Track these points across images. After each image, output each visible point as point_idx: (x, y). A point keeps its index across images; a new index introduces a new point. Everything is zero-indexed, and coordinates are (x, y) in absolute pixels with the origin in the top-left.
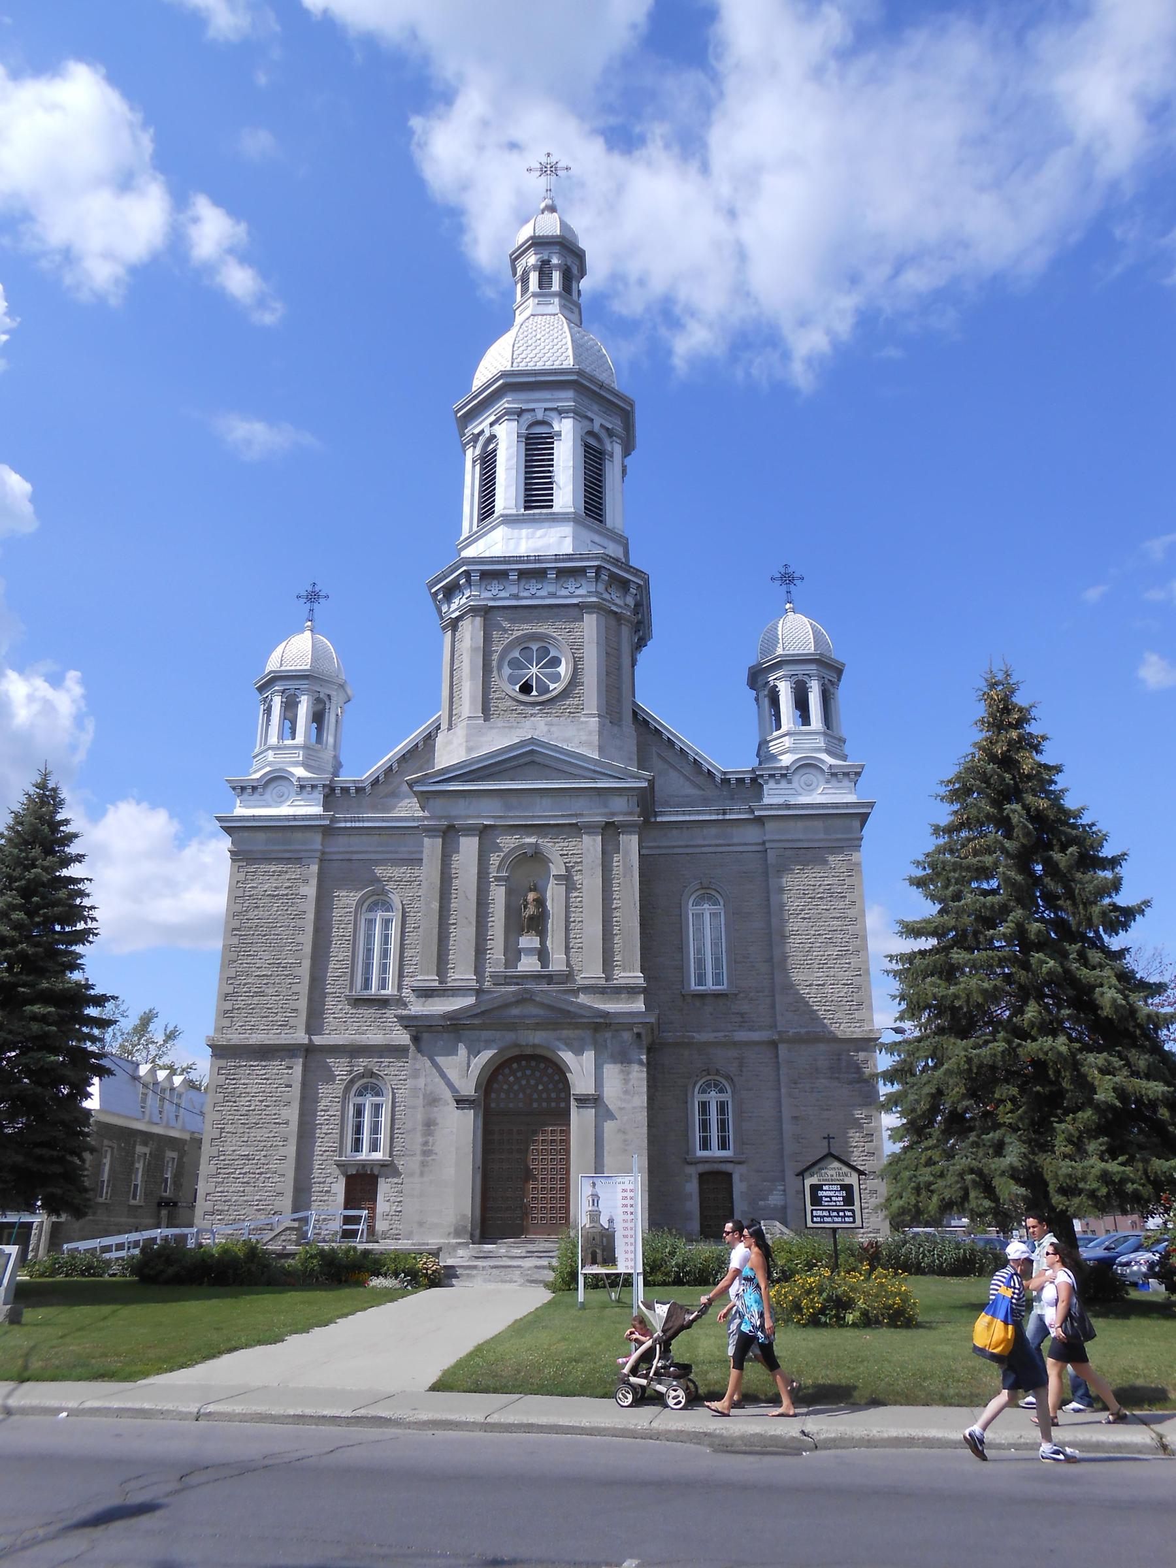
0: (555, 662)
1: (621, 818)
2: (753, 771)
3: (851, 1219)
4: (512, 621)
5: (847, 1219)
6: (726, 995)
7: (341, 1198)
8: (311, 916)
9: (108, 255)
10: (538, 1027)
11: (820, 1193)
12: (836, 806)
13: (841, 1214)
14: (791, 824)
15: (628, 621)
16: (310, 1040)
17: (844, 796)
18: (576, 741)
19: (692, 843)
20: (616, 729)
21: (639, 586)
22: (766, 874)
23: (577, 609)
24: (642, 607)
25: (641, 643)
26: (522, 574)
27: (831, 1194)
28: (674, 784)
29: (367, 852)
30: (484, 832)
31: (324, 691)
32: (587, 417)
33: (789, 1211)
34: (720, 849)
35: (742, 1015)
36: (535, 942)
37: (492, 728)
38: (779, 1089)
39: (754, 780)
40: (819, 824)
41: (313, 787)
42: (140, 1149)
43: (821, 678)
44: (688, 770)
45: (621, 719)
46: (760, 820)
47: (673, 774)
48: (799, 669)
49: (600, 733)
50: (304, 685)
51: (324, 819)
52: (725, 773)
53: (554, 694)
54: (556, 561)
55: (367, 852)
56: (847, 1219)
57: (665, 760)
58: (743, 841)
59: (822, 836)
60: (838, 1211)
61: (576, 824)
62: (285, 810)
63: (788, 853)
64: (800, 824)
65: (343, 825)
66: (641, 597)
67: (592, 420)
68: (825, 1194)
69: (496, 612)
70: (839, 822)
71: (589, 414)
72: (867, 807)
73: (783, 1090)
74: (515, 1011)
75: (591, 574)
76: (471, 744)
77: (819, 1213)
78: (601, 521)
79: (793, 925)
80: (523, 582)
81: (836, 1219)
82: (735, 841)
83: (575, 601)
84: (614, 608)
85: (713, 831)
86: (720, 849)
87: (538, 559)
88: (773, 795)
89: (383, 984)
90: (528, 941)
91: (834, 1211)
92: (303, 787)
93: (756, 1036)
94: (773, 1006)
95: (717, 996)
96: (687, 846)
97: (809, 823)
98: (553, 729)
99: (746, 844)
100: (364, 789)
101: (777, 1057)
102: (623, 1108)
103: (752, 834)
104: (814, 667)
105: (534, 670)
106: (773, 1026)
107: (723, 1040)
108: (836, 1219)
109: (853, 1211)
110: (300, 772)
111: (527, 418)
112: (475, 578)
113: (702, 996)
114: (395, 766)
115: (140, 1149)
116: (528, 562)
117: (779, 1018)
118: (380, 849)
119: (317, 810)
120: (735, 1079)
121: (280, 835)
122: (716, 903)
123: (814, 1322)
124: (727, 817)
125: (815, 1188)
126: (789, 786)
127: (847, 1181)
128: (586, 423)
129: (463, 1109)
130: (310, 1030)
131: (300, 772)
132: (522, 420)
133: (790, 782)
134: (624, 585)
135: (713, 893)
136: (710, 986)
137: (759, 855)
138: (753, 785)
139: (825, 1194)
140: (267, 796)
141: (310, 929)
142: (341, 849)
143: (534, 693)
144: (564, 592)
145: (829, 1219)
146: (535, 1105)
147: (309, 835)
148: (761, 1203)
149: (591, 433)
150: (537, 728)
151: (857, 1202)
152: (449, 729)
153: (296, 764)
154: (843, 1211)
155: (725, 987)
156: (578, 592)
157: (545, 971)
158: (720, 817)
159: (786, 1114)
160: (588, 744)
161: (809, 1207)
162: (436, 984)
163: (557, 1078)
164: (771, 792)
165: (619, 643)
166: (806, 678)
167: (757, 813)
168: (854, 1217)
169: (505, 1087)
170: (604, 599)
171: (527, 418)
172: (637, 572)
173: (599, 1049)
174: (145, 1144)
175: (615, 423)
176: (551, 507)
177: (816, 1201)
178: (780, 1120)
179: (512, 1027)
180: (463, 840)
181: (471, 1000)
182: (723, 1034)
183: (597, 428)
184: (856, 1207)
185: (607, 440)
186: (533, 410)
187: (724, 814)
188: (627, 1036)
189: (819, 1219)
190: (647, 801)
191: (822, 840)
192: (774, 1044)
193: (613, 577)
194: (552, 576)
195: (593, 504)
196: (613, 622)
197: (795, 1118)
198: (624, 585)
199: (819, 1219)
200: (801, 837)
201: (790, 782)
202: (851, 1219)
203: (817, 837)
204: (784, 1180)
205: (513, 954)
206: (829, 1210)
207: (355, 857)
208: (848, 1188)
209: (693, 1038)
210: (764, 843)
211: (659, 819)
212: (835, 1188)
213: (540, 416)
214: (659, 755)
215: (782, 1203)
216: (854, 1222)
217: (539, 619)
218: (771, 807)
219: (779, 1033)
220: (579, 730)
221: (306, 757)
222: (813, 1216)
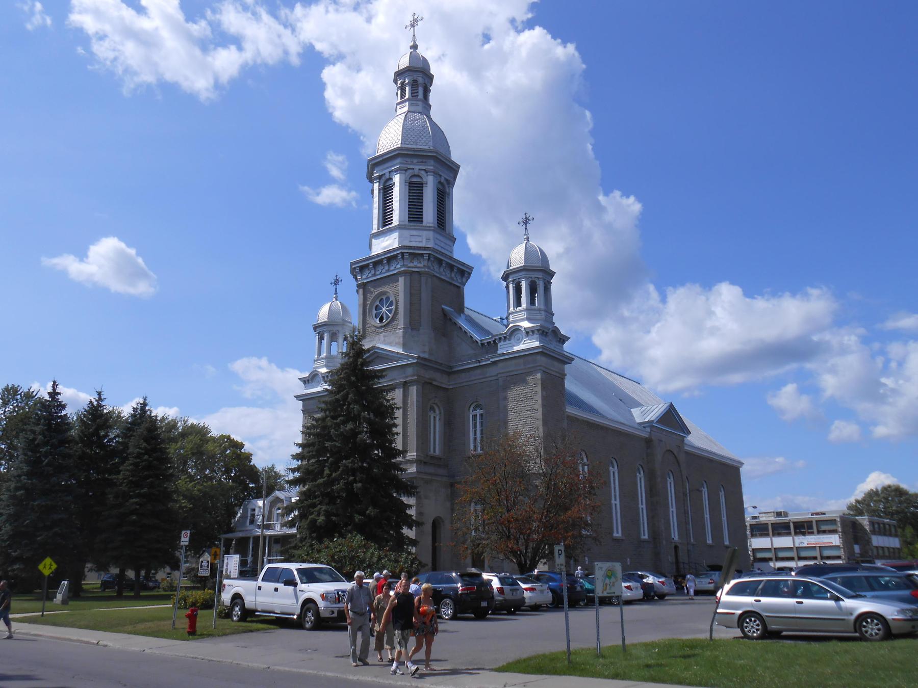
4: (374, 287)
9: (526, 13)
12: (530, 349)
31: (335, 329)
41: (533, 332)
43: (526, 278)
48: (533, 275)
49: (404, 337)
50: (325, 328)
62: (522, 347)
64: (514, 362)
79: (511, 416)
82: (488, 375)
89: (476, 450)
92: (529, 332)
104: (523, 273)
110: (526, 324)
111: (410, 172)
112: (406, 256)
119: (537, 344)
123: (223, 618)
131: (526, 324)
140: (512, 341)
153: (523, 320)
160: (397, 344)
171: (410, 172)
217: (384, 284)
218: (503, 354)
221: (327, 362)
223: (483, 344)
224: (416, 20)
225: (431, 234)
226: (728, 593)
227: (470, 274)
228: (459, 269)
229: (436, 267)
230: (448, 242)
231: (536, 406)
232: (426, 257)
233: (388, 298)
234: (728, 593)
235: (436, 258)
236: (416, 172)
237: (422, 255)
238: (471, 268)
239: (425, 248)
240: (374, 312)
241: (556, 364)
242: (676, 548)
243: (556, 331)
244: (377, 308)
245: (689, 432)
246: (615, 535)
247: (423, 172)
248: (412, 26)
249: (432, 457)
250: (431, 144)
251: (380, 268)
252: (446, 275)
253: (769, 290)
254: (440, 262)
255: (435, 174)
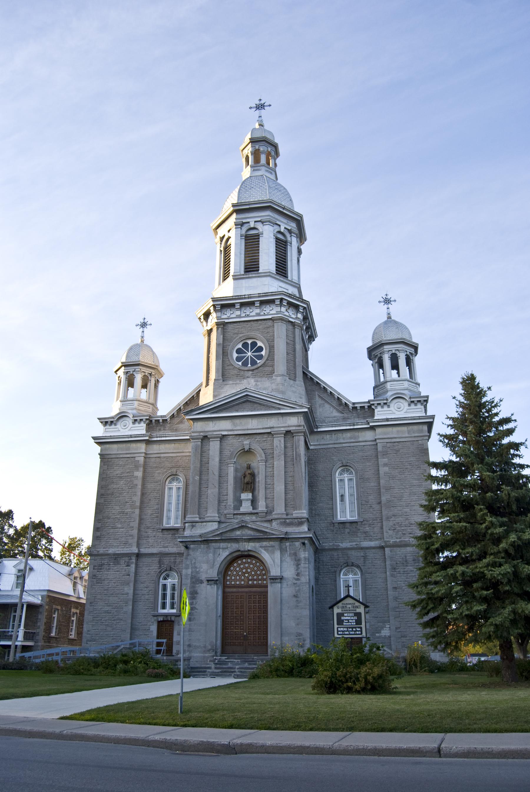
0: (260, 349)
1: (294, 428)
2: (369, 402)
3: (360, 633)
5: (357, 633)
6: (356, 522)
7: (155, 633)
8: (140, 487)
10: (250, 540)
11: (343, 618)
13: (354, 629)
14: (390, 429)
15: (298, 326)
16: (139, 551)
17: (417, 412)
18: (270, 389)
19: (337, 442)
20: (292, 382)
21: (304, 308)
22: (377, 457)
23: (271, 321)
24: (308, 317)
25: (312, 338)
26: (242, 305)
27: (349, 618)
28: (325, 411)
29: (168, 453)
30: (223, 437)
32: (277, 224)
33: (392, 639)
34: (352, 444)
35: (365, 533)
36: (250, 496)
37: (226, 384)
38: (386, 573)
39: (369, 407)
40: (405, 428)
42: (73, 610)
44: (335, 403)
45: (295, 377)
46: (373, 428)
47: (327, 406)
51: (146, 436)
52: (354, 404)
53: (259, 365)
54: (259, 297)
55: (168, 453)
56: (357, 633)
57: (322, 399)
58: (364, 439)
59: (407, 435)
60: (352, 628)
61: (270, 433)
63: (388, 445)
64: (395, 429)
65: (156, 439)
66: (307, 313)
67: (280, 226)
68: (345, 618)
69: (229, 325)
70: (415, 427)
71: (278, 223)
72: (430, 418)
73: (388, 573)
74: (238, 533)
75: (278, 302)
76: (216, 393)
77: (342, 629)
78: (285, 277)
80: (243, 309)
81: (351, 633)
82: (360, 439)
83: (270, 317)
84: (291, 320)
85: (348, 435)
86: (352, 444)
87: (250, 296)
88: (380, 414)
90: (246, 496)
91: (350, 628)
93: (373, 544)
94: (382, 528)
95: (352, 523)
96: (335, 444)
97: (411, 427)
98: (259, 383)
99: (366, 441)
100: (166, 420)
101: (385, 555)
102: (296, 583)
103: (369, 435)
105: (249, 354)
106: (382, 538)
107: (355, 546)
108: (351, 633)
109: (361, 628)
112: (285, 303)
113: (343, 523)
114: (182, 408)
115: (73, 610)
116: (245, 298)
117: (385, 534)
118: (175, 451)
120: (362, 567)
121: (173, 445)
122: (351, 473)
124: (356, 427)
125: (339, 615)
126: (389, 409)
127: (358, 610)
128: (276, 227)
129: (211, 585)
130: (138, 546)
132: (243, 228)
133: (389, 406)
134: (296, 307)
135: (350, 468)
136: (348, 517)
137: (373, 447)
138: (367, 410)
139: (345, 618)
140: (118, 426)
141: (139, 494)
142: (155, 452)
143: (249, 365)
144: (225, 317)
145: (347, 633)
146: (250, 582)
147: (139, 445)
148: (377, 635)
149: (279, 232)
150: (250, 384)
151: (363, 623)
152: (206, 387)
154: (355, 628)
155: (356, 518)
156: (271, 312)
157: (255, 511)
158: (352, 427)
159: (390, 586)
161: (336, 626)
162: (198, 519)
163: (261, 568)
164: (379, 413)
165: (294, 337)
166: (397, 352)
167: (371, 424)
168: (361, 631)
169: (235, 573)
170: (285, 315)
172: (304, 301)
173: (283, 551)
174: (77, 608)
175: (293, 226)
176: (259, 270)
177: (340, 622)
178: (387, 589)
179: (236, 540)
180: (211, 443)
181: (215, 526)
182: (355, 543)
183: (282, 230)
184: (363, 626)
185: (288, 235)
186: (249, 222)
187: (354, 425)
188: (298, 544)
189: (341, 633)
190: (309, 418)
191: (407, 437)
192: (382, 548)
193: (290, 304)
194: (257, 304)
195: (282, 269)
196: (291, 327)
197: (395, 588)
198: (296, 307)
199: (341, 633)
200: (395, 436)
201: (389, 406)
202: (360, 633)
203: (404, 436)
204: (389, 622)
205: (239, 502)
206: (347, 628)
207: (162, 455)
208: (359, 615)
209: (339, 545)
210: (375, 440)
211: (319, 430)
212: (351, 615)
213: (252, 225)
214: (319, 396)
215: (389, 634)
216: (361, 634)
218: (378, 420)
219: (385, 542)
220: (272, 383)
222: (338, 631)
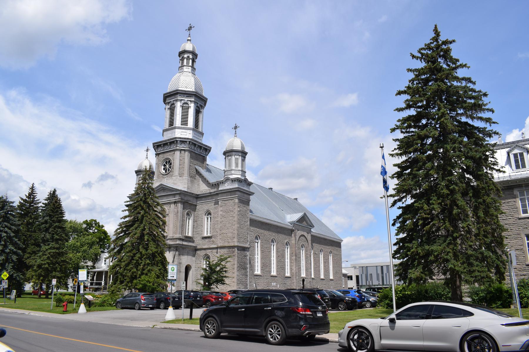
89: (207, 234)
112: (178, 142)
218: (221, 190)
223: (213, 185)
224: (191, 27)
225: (191, 132)
226: (396, 310)
227: (210, 151)
228: (204, 148)
229: (193, 147)
230: (200, 135)
231: (234, 215)
232: (188, 143)
233: (169, 161)
234: (396, 310)
235: (193, 143)
236: (186, 102)
237: (186, 142)
238: (211, 148)
239: (188, 139)
240: (163, 167)
241: (245, 195)
242: (303, 281)
243: (246, 180)
244: (165, 165)
245: (313, 227)
246: (272, 274)
247: (190, 102)
248: (189, 30)
249: (187, 237)
250: (193, 88)
251: (166, 147)
252: (198, 151)
253: (112, 219)
254: (195, 145)
255: (195, 102)
